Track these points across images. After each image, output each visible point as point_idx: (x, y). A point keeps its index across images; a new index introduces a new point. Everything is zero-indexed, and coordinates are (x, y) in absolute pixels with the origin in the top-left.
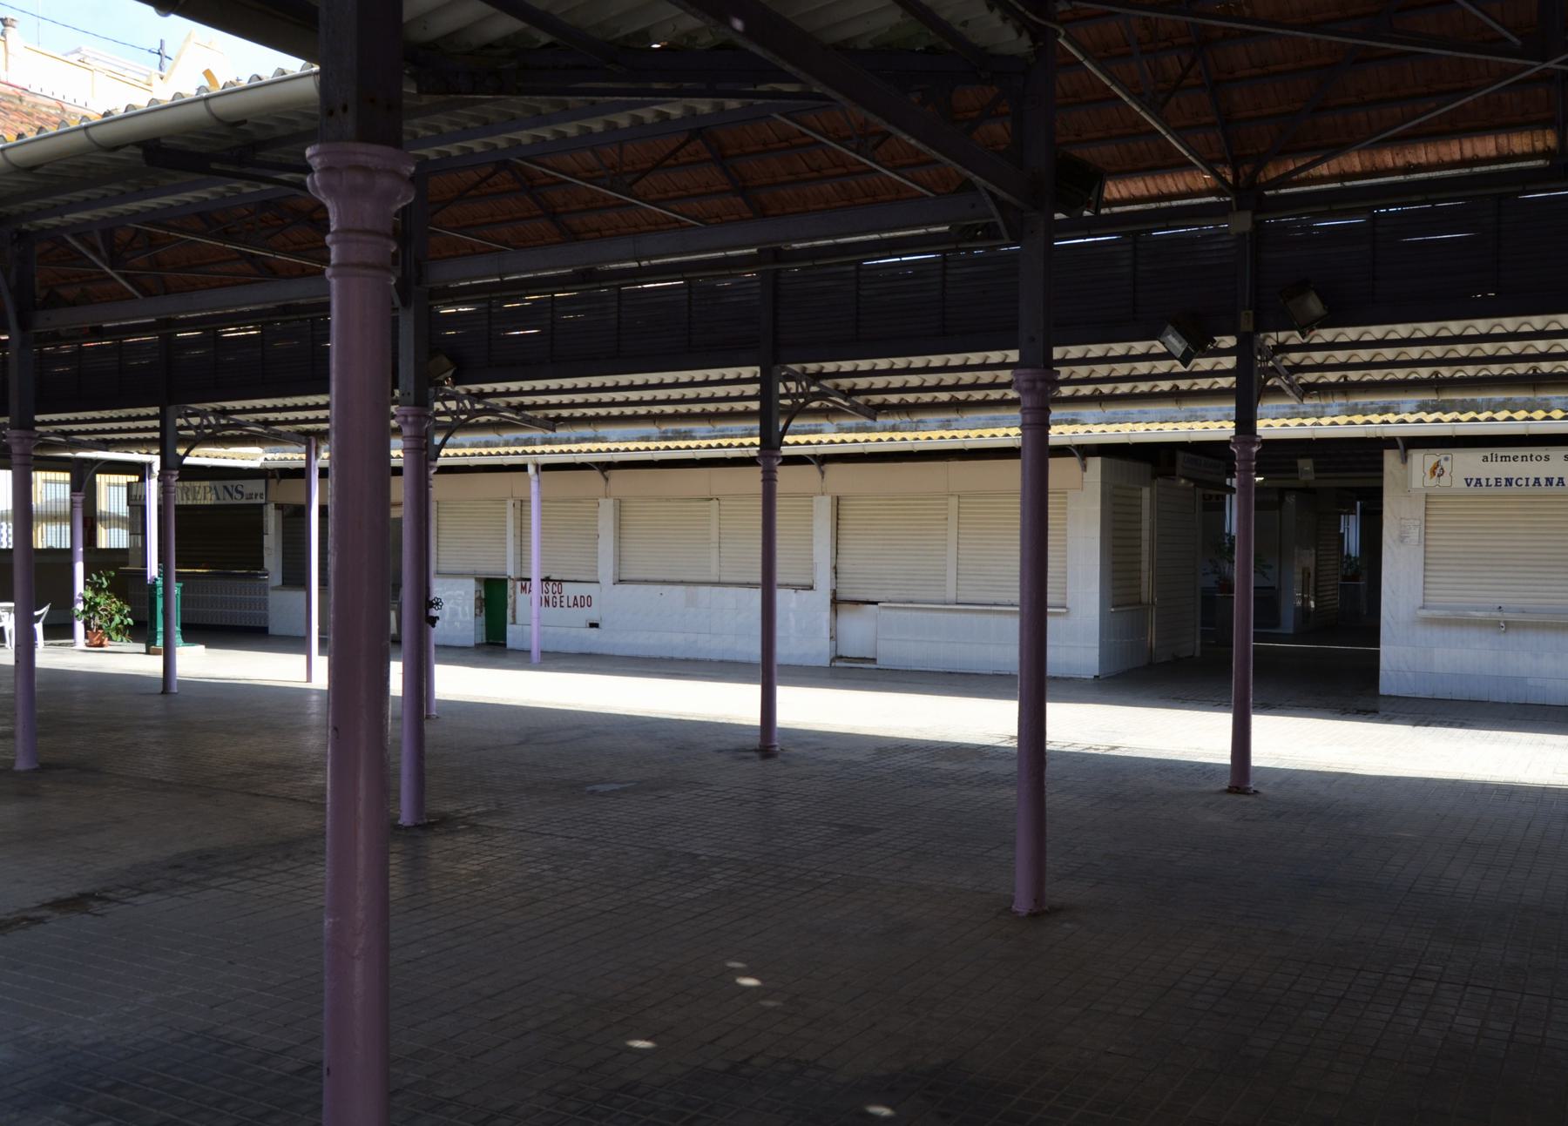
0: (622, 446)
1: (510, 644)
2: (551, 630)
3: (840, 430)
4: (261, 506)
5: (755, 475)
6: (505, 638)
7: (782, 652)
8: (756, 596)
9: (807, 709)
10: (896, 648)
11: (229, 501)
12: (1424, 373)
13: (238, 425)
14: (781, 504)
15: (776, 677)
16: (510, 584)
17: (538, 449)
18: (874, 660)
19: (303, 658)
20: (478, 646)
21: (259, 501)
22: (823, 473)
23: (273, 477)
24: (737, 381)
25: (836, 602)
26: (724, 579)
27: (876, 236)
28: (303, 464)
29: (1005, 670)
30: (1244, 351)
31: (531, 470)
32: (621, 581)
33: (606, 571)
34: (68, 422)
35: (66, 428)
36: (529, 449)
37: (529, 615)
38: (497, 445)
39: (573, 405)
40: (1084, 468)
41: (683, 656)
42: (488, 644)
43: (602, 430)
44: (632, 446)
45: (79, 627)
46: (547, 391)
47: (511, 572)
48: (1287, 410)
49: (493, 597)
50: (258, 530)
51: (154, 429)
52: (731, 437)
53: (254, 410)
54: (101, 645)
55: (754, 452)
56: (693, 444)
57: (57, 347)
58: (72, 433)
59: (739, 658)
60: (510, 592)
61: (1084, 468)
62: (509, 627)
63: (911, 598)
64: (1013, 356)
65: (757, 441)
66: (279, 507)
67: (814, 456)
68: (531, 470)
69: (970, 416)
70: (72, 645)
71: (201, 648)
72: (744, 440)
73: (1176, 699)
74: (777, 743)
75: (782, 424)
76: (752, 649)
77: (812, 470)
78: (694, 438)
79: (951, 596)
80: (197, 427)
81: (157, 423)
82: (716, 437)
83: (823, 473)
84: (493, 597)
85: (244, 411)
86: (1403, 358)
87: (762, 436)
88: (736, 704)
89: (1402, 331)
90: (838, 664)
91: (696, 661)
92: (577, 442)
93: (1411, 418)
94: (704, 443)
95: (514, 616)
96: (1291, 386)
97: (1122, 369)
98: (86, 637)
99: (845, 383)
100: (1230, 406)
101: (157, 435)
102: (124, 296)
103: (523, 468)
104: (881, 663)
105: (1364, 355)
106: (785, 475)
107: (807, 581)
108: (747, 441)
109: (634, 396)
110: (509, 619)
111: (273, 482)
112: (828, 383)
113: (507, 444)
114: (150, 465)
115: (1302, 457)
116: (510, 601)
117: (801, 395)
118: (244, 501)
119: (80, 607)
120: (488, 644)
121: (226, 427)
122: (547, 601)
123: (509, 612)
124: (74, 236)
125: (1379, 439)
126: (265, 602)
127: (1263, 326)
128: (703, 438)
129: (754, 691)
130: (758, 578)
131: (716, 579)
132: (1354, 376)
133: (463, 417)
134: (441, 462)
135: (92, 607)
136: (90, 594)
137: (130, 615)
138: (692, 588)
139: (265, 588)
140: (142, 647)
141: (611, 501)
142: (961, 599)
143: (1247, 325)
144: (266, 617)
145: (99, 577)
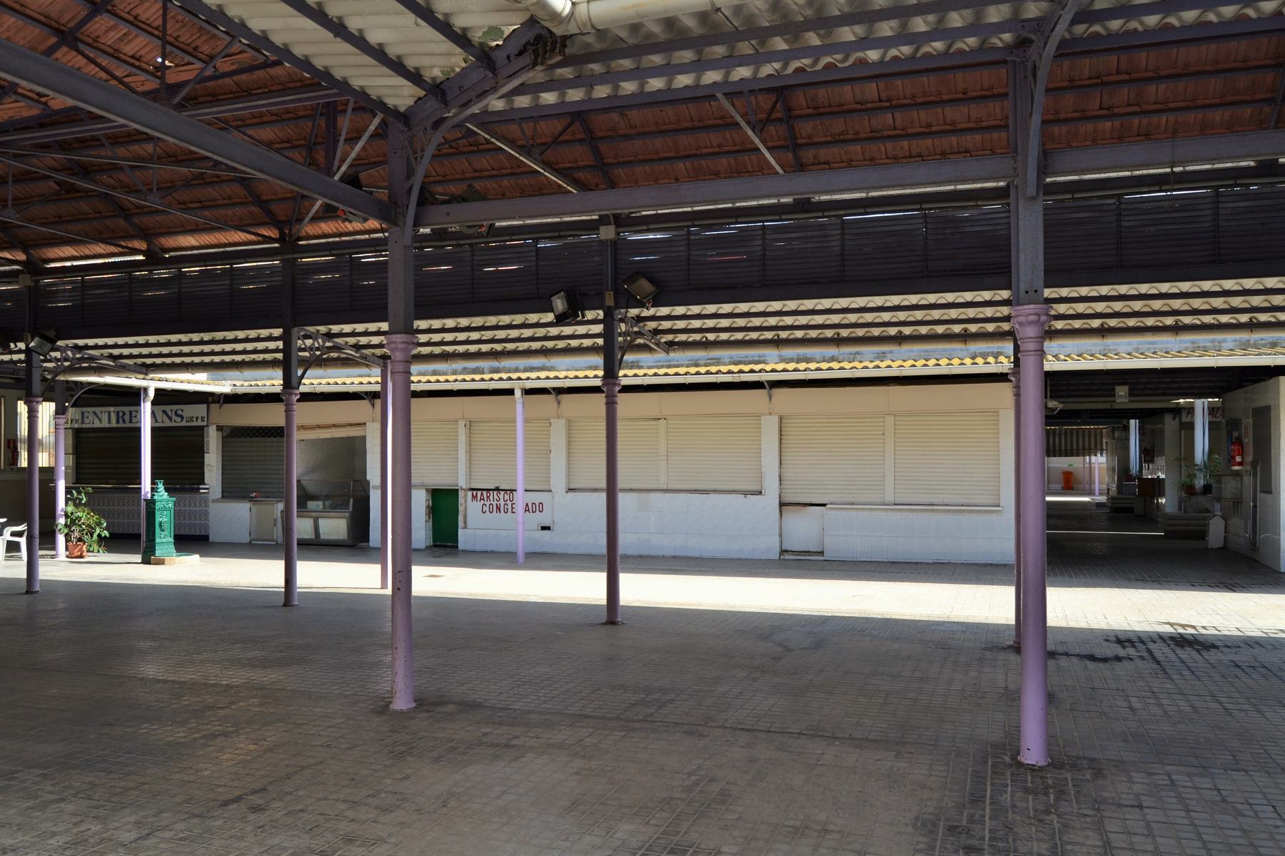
0: (572, 374)
1: (461, 546)
2: (504, 533)
3: (783, 360)
4: (201, 428)
5: (600, 399)
6: (457, 541)
7: (626, 541)
8: (603, 497)
9: (640, 590)
10: (839, 544)
11: (168, 424)
12: (893, 331)
13: (92, 359)
14: (621, 426)
15: (619, 566)
16: (461, 494)
17: (524, 375)
18: (822, 553)
19: (378, 568)
20: (428, 548)
21: (200, 423)
22: (559, 403)
23: (214, 402)
24: (268, 339)
25: (782, 505)
26: (670, 487)
27: (1128, 174)
28: (378, 388)
29: (594, 551)
30: (609, 321)
31: (518, 393)
32: (570, 490)
33: (558, 481)
34: (116, 346)
35: (116, 352)
36: (514, 376)
37: (475, 522)
38: (445, 374)
39: (202, 354)
40: (373, 405)
41: (636, 553)
42: (435, 546)
43: (1112, 342)
44: (581, 374)
45: (61, 539)
46: (236, 341)
47: (462, 483)
48: (1189, 345)
49: (444, 504)
50: (200, 450)
51: (276, 351)
52: (678, 366)
53: (106, 346)
54: (81, 557)
55: (598, 382)
56: (640, 372)
57: (151, 271)
58: (121, 357)
59: (691, 554)
60: (461, 500)
61: (373, 405)
62: (460, 531)
63: (853, 500)
64: (384, 326)
65: (601, 373)
66: (220, 428)
67: (366, 393)
68: (518, 393)
69: (906, 348)
70: (53, 557)
71: (197, 556)
72: (588, 371)
73: (1130, 580)
74: (37, 588)
75: (300, 372)
76: (600, 544)
77: (550, 399)
78: (640, 368)
79: (889, 497)
80: (311, 349)
81: (280, 344)
82: (662, 367)
83: (559, 403)
84: (444, 504)
85: (96, 347)
86: (781, 324)
87: (605, 370)
88: (586, 588)
89: (776, 306)
90: (787, 557)
91: (649, 557)
92: (525, 370)
93: (871, 365)
94: (651, 372)
95: (465, 522)
96: (658, 344)
97: (725, 323)
98: (67, 549)
99: (652, 325)
100: (598, 360)
101: (600, 341)
102: (544, 190)
103: (510, 392)
104: (827, 556)
105: (1218, 303)
106: (623, 400)
107: (757, 488)
108: (591, 373)
109: (501, 334)
110: (461, 524)
111: (214, 407)
112: (340, 341)
113: (454, 373)
114: (146, 389)
115: (1120, 384)
116: (461, 508)
117: (318, 349)
118: (184, 424)
119: (62, 521)
120: (435, 546)
121: (330, 349)
122: (498, 508)
123: (461, 518)
124: (482, 126)
125: (1269, 367)
126: (206, 513)
127: (618, 306)
128: (650, 368)
129: (601, 578)
130: (604, 485)
131: (665, 487)
132: (784, 334)
133: (318, 353)
134: (303, 389)
135: (72, 521)
136: (70, 509)
137: (107, 529)
138: (644, 495)
139: (206, 501)
140: (138, 558)
141: (563, 422)
142: (899, 500)
143: (609, 301)
144: (207, 527)
145: (79, 493)
